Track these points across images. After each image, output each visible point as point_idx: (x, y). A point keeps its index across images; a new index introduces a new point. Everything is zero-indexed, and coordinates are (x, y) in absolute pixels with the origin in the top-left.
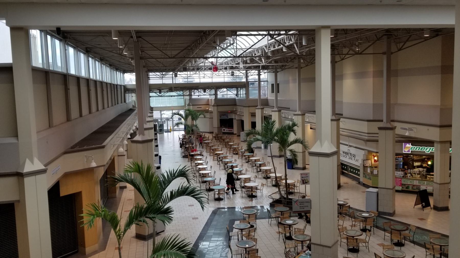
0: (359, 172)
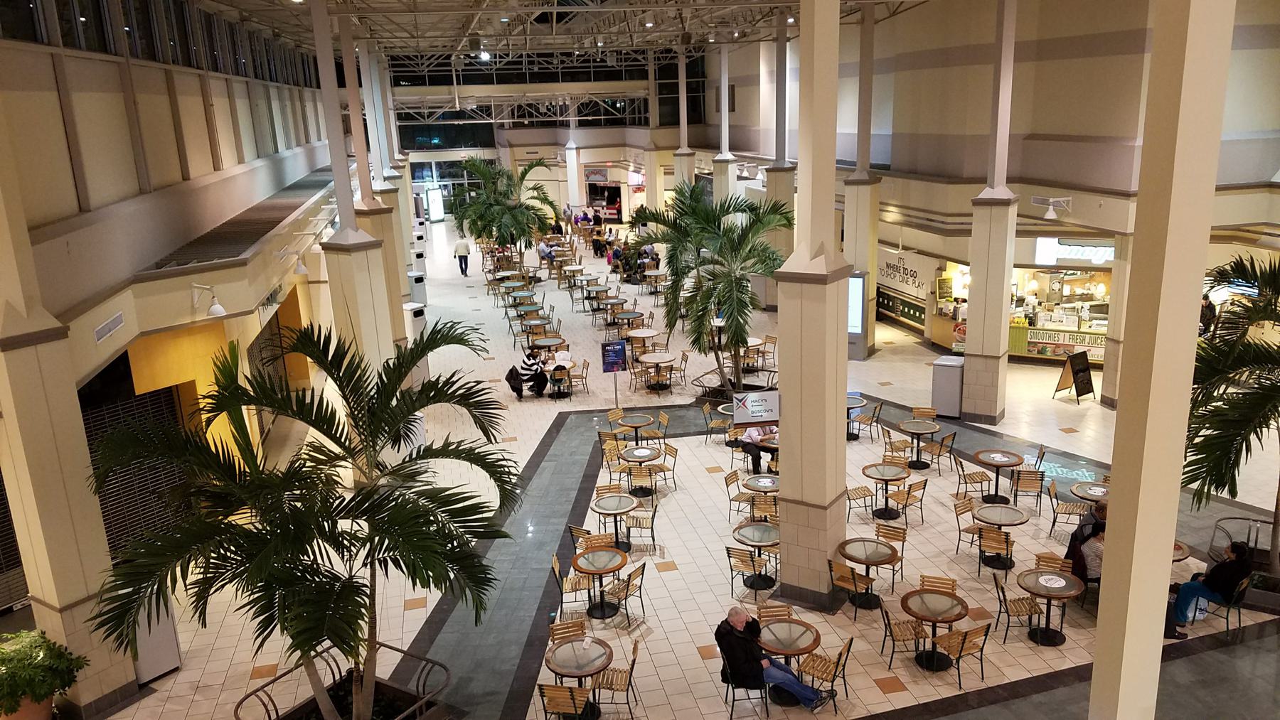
0: (924, 313)
